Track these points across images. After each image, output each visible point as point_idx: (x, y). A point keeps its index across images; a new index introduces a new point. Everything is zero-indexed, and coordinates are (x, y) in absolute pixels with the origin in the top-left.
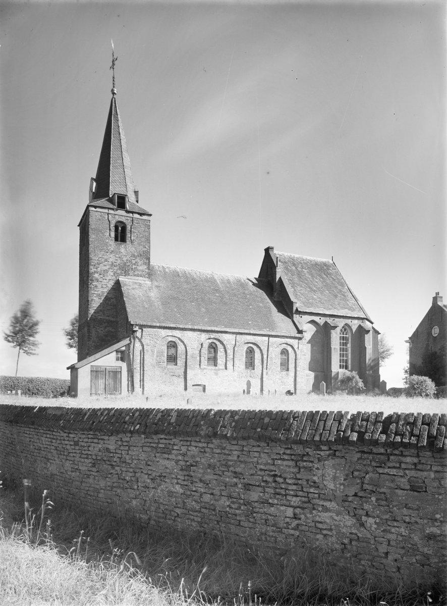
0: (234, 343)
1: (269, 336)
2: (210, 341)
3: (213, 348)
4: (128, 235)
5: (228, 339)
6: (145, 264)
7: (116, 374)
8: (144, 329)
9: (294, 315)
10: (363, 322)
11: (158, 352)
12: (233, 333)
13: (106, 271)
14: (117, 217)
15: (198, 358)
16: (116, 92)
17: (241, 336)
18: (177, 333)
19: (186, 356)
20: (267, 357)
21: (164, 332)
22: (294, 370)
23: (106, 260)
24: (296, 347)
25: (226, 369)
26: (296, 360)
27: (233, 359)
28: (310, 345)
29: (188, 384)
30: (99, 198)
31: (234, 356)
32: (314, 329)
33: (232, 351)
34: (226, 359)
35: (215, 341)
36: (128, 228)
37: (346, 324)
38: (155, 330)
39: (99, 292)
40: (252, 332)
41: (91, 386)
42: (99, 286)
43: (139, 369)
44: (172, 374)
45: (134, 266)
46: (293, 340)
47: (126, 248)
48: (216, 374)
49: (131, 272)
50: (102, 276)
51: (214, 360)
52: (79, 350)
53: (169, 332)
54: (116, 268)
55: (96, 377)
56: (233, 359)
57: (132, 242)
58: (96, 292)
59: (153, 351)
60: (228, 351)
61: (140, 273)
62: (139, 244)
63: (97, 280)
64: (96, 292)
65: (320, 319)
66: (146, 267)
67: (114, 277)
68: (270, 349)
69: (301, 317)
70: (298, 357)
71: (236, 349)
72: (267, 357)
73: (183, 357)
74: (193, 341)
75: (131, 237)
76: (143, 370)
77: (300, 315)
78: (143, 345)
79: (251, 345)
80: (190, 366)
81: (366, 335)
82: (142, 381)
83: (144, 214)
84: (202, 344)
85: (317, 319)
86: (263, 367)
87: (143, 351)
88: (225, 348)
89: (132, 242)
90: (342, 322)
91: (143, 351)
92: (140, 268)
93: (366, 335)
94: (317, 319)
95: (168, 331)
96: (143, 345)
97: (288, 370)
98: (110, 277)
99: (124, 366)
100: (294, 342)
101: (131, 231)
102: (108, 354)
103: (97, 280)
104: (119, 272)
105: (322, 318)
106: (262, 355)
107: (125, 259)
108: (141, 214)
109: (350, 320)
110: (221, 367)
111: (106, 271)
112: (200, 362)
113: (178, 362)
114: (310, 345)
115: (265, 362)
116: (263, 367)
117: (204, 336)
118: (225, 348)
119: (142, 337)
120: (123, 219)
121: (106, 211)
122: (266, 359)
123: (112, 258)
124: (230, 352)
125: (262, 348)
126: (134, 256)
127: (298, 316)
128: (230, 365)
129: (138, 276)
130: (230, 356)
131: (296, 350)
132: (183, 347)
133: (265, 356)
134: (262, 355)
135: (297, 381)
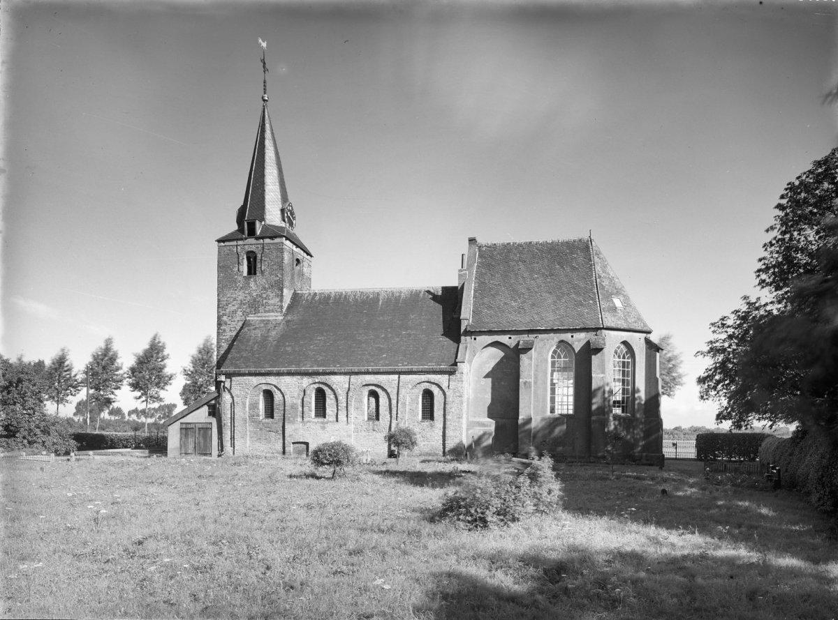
0: (347, 386)
1: (399, 373)
2: (316, 386)
3: (321, 395)
4: (258, 265)
5: (339, 382)
6: (277, 296)
7: (205, 430)
8: (233, 378)
9: (463, 338)
10: (596, 335)
11: (250, 404)
12: (345, 374)
13: (235, 312)
14: (246, 247)
15: (300, 409)
16: (266, 98)
17: (356, 377)
18: (272, 380)
19: (285, 406)
20: (397, 402)
21: (255, 380)
22: (442, 419)
23: (235, 299)
24: (444, 386)
25: (337, 421)
26: (445, 404)
27: (347, 407)
28: (489, 380)
29: (286, 442)
30: (264, 210)
31: (347, 404)
32: (502, 354)
33: (345, 397)
34: (337, 407)
35: (321, 386)
36: (259, 256)
37: (562, 341)
38: (245, 378)
39: (227, 337)
40: (370, 369)
41: (181, 446)
42: (228, 330)
43: (229, 424)
44: (268, 429)
45: (264, 301)
46: (439, 376)
47: (255, 281)
48: (323, 428)
49: (261, 309)
50: (230, 318)
51: (321, 410)
52: (659, 423)
53: (262, 379)
54: (244, 307)
55: (186, 435)
56: (347, 407)
57: (262, 272)
58: (224, 337)
59: (244, 404)
60: (340, 398)
61: (271, 308)
62: (271, 274)
63: (226, 324)
64: (224, 337)
65: (510, 338)
66: (278, 299)
67: (243, 317)
68: (402, 391)
69: (475, 339)
70: (449, 399)
71: (350, 394)
72: (397, 402)
73: (281, 409)
74: (292, 388)
75: (261, 267)
76: (234, 427)
77: (473, 337)
78: (233, 397)
79: (373, 388)
80: (289, 419)
81: (593, 357)
82: (233, 438)
83: (276, 237)
84: (304, 391)
85: (504, 339)
86: (391, 417)
87: (233, 404)
88: (335, 394)
89: (262, 272)
90: (553, 339)
91: (233, 404)
92: (271, 302)
93: (593, 357)
94: (504, 339)
95: (260, 378)
96: (233, 397)
97: (432, 418)
98: (238, 319)
99: (214, 421)
100: (443, 379)
101: (261, 260)
102: (198, 409)
103: (226, 324)
104: (248, 310)
105: (513, 337)
106: (390, 400)
107: (254, 294)
108: (271, 238)
109: (569, 335)
110: (330, 419)
111: (235, 312)
112: (303, 414)
113: (275, 415)
114: (489, 380)
115: (394, 412)
116: (391, 417)
117: (306, 381)
118: (335, 394)
119: (231, 387)
120: (253, 248)
121: (235, 243)
122: (396, 405)
123: (240, 295)
124: (342, 398)
125: (389, 391)
126: (264, 288)
127: (468, 338)
128: (342, 416)
129: (269, 311)
130: (343, 404)
131: (446, 390)
132: (280, 395)
133: (394, 402)
134: (390, 400)
135: (447, 435)
